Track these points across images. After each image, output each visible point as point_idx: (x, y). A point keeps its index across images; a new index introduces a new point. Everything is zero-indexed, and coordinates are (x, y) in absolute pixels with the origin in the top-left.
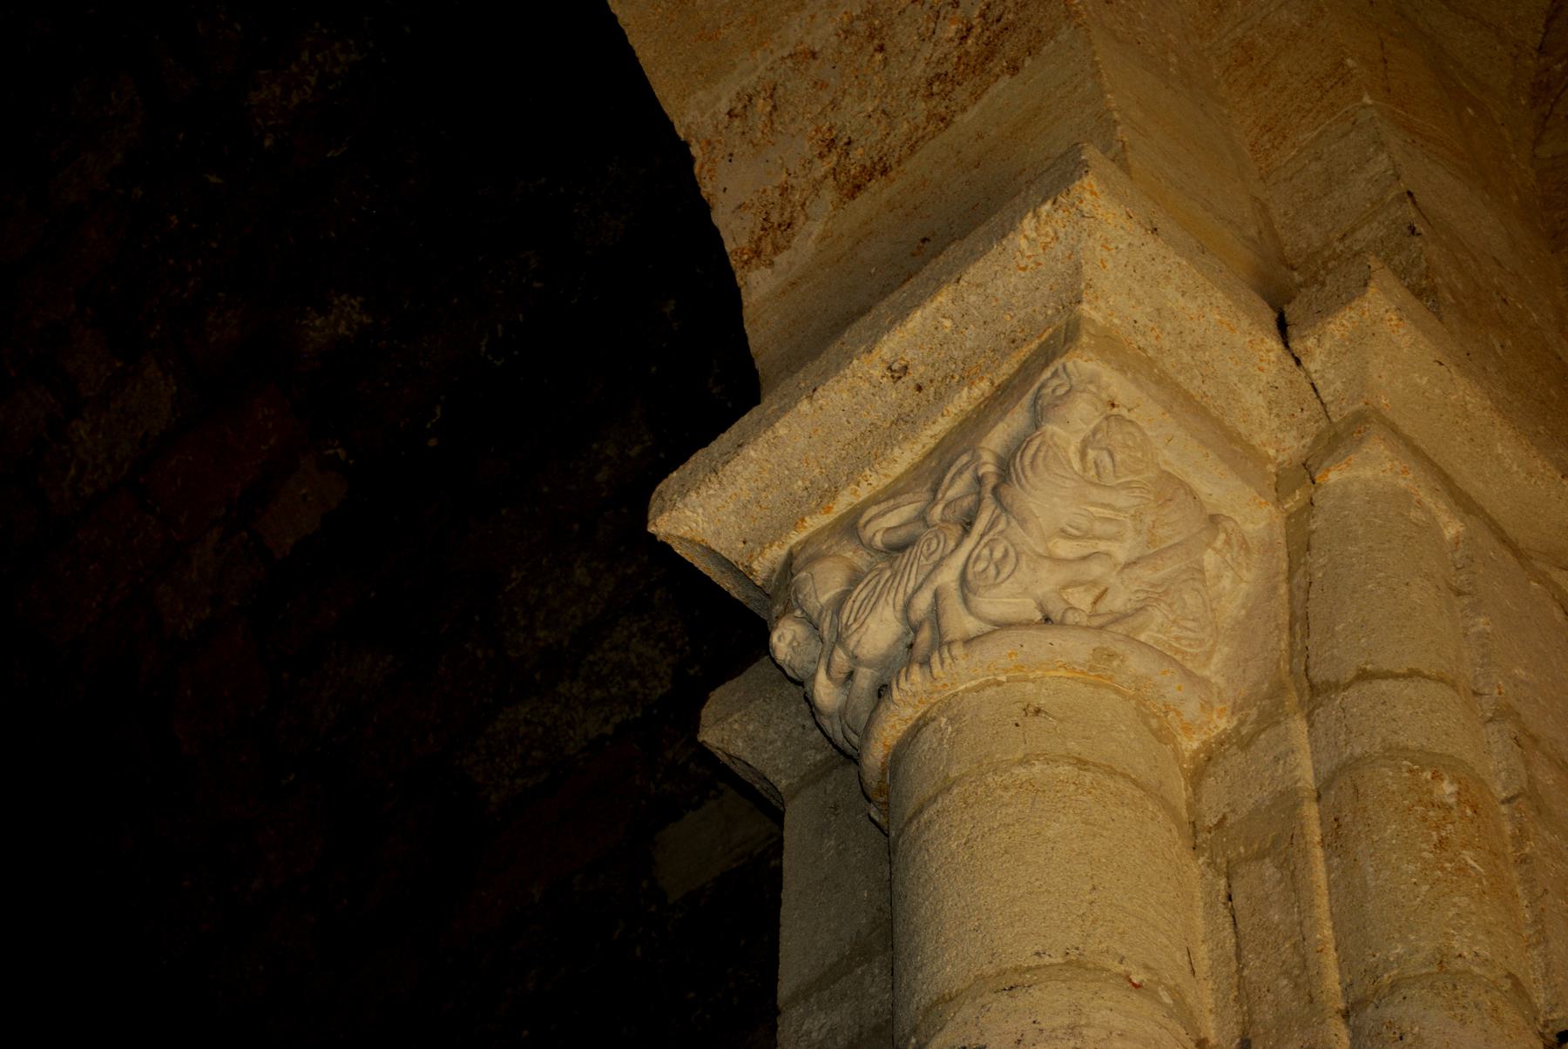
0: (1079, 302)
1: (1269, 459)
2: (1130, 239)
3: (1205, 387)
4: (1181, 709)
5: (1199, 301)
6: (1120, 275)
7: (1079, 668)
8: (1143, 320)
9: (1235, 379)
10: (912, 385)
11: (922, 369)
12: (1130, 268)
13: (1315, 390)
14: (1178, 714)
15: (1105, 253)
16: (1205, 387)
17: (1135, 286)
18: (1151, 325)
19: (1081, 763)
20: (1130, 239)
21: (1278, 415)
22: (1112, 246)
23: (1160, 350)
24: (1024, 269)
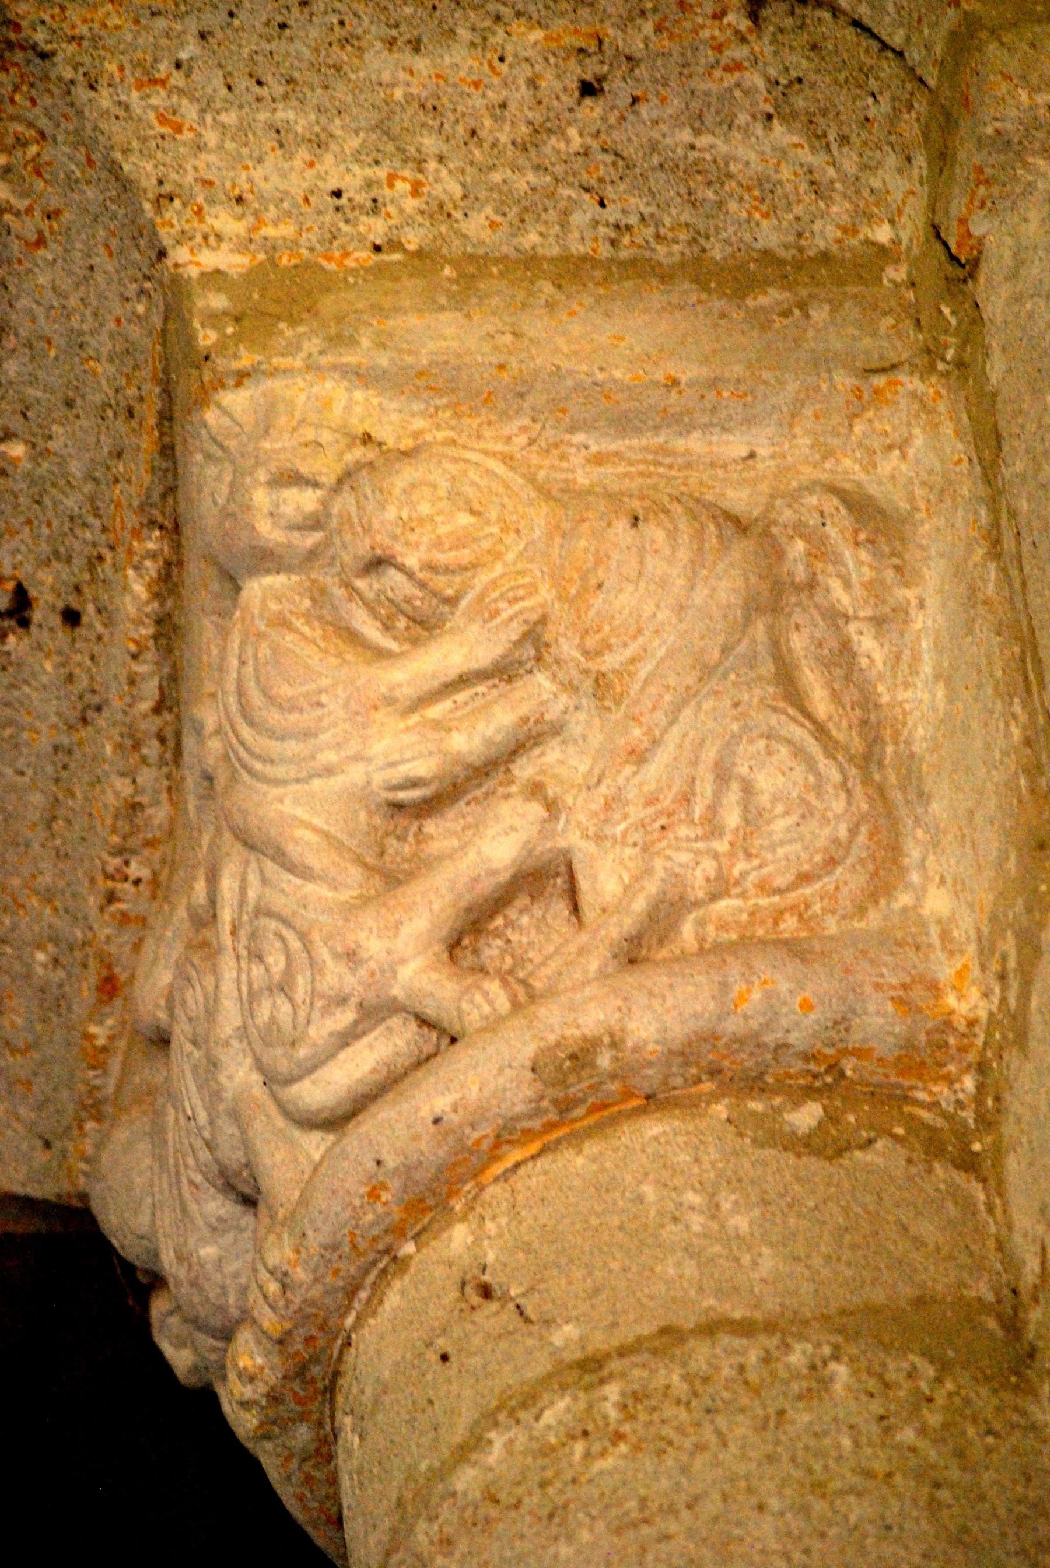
0: (162, 254)
1: (884, 254)
2: (192, 25)
3: (612, 213)
4: (855, 1039)
5: (464, 34)
6: (230, 118)
7: (536, 1124)
8: (352, 180)
9: (686, 136)
10: (56, 621)
11: (46, 577)
12: (242, 83)
13: (867, 30)
14: (860, 1053)
15: (159, 98)
16: (612, 213)
17: (285, 114)
18: (381, 173)
19: (591, 1368)
20: (192, 25)
21: (844, 140)
22: (164, 68)
23: (441, 211)
24: (41, 242)
